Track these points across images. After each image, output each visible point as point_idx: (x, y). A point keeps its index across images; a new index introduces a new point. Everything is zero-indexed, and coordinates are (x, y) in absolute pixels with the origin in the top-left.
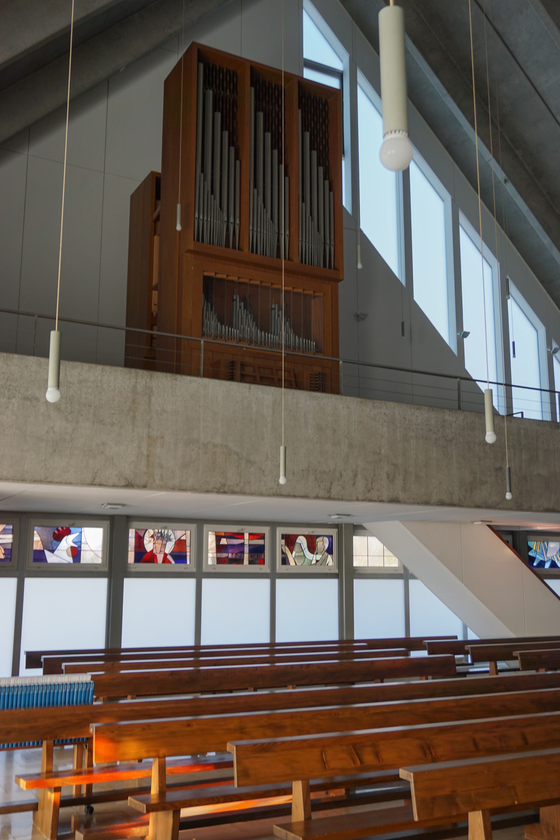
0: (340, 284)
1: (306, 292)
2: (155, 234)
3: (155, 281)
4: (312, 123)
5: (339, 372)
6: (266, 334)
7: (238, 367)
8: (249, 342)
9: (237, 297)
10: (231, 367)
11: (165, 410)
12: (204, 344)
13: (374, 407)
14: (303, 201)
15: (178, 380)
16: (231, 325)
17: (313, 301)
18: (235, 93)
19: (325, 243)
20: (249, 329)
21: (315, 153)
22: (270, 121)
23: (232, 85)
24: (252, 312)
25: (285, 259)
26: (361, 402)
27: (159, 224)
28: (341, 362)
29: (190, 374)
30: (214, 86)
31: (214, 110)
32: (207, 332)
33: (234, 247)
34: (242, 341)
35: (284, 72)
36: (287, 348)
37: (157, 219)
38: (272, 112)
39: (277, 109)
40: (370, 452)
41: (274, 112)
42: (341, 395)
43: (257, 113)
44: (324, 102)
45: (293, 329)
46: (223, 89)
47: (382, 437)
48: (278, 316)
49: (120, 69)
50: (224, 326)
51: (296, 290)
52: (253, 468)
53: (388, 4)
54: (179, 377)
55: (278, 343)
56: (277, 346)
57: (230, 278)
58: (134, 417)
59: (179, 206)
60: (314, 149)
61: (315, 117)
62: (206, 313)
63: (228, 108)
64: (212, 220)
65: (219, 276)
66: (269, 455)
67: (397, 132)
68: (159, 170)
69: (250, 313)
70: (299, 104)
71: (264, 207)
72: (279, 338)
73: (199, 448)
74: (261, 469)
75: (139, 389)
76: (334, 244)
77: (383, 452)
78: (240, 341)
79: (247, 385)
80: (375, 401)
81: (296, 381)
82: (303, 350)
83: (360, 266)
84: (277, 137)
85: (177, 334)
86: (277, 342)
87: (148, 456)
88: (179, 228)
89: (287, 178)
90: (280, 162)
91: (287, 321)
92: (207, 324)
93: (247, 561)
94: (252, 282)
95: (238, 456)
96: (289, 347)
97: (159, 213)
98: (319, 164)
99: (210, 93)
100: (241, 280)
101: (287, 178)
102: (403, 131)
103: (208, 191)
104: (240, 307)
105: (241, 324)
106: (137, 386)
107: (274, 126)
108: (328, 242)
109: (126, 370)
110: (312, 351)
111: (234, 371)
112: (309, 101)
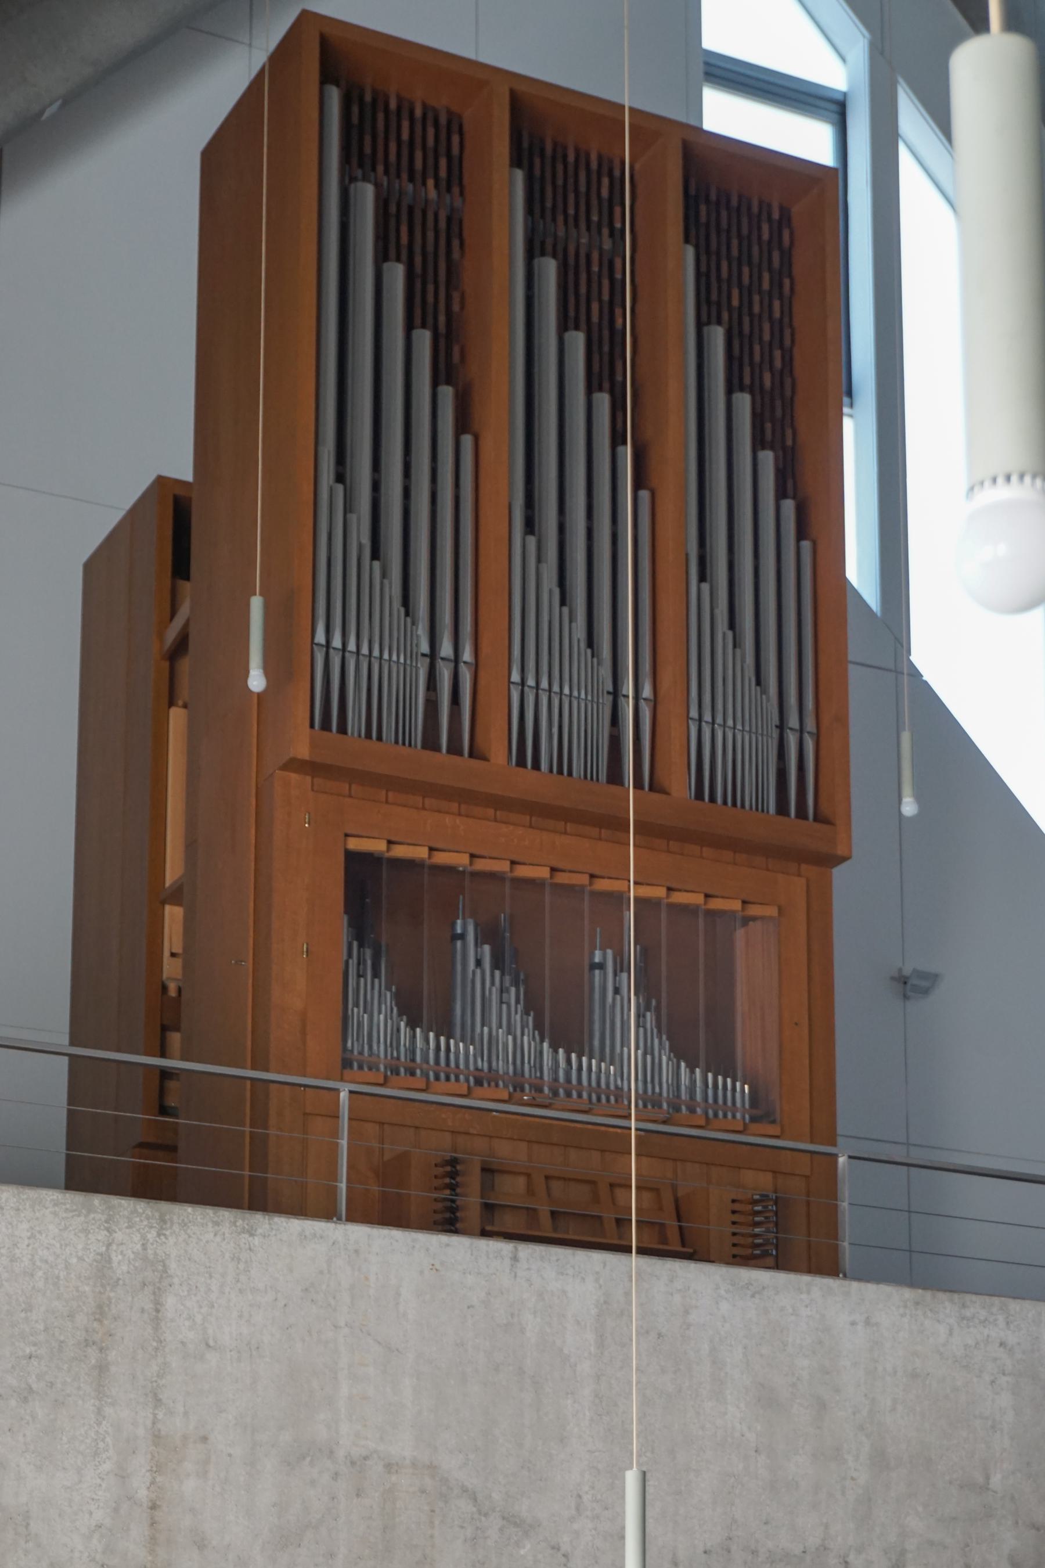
0: (839, 874)
1: (716, 904)
2: (171, 703)
3: (173, 871)
4: (735, 292)
5: (835, 1197)
6: (573, 1056)
7: (472, 1181)
8: (511, 1089)
9: (466, 926)
10: (447, 1180)
11: (211, 1343)
12: (350, 1099)
13: (963, 1318)
14: (702, 578)
15: (259, 1231)
16: (445, 1027)
17: (740, 934)
18: (456, 190)
19: (781, 727)
20: (510, 1038)
21: (744, 402)
22: (583, 290)
23: (443, 163)
24: (522, 977)
25: (638, 785)
26: (917, 1303)
27: (185, 665)
28: (842, 1160)
29: (299, 1210)
30: (380, 168)
31: (382, 256)
32: (361, 1053)
33: (455, 749)
34: (486, 1085)
35: (631, 109)
36: (649, 1107)
37: (181, 646)
38: (588, 257)
39: (607, 245)
40: (950, 1483)
41: (595, 256)
42: (845, 1276)
43: (536, 261)
44: (776, 216)
45: (668, 1039)
46: (411, 179)
47: (993, 1427)
48: (617, 991)
49: (42, 112)
50: (422, 1031)
51: (679, 898)
52: (528, 1546)
53: (979, 24)
54: (260, 1221)
55: (617, 1087)
56: (612, 1099)
57: (441, 858)
58: (102, 1368)
59: (256, 603)
60: (742, 389)
61: (746, 270)
62: (358, 984)
63: (430, 248)
64: (376, 653)
65: (400, 852)
66: (586, 1498)
67: (1014, 478)
68: (183, 469)
69: (516, 983)
70: (686, 218)
71: (563, 602)
72: (618, 1074)
73: (336, 1476)
74: (559, 1549)
75: (120, 1266)
76: (814, 730)
77: (996, 1480)
78: (479, 1082)
79: (506, 1247)
80: (969, 1298)
81: (680, 1227)
82: (706, 1114)
83: (909, 807)
84: (606, 348)
85: (254, 1068)
86: (612, 1087)
87: (154, 1507)
88: (257, 682)
89: (644, 495)
90: (617, 439)
91: (648, 1008)
92: (360, 1025)
93: (574, 1254)
94: (523, 872)
95: (475, 1500)
96: (656, 1104)
97: (186, 625)
98: (759, 442)
99: (366, 194)
100: (481, 865)
101: (644, 495)
102: (1034, 477)
103: (360, 546)
104: (479, 963)
105: (483, 1025)
106: (113, 1255)
107: (595, 307)
108: (793, 721)
109: (75, 1199)
110: (738, 1116)
111: (458, 1179)
112: (724, 214)
